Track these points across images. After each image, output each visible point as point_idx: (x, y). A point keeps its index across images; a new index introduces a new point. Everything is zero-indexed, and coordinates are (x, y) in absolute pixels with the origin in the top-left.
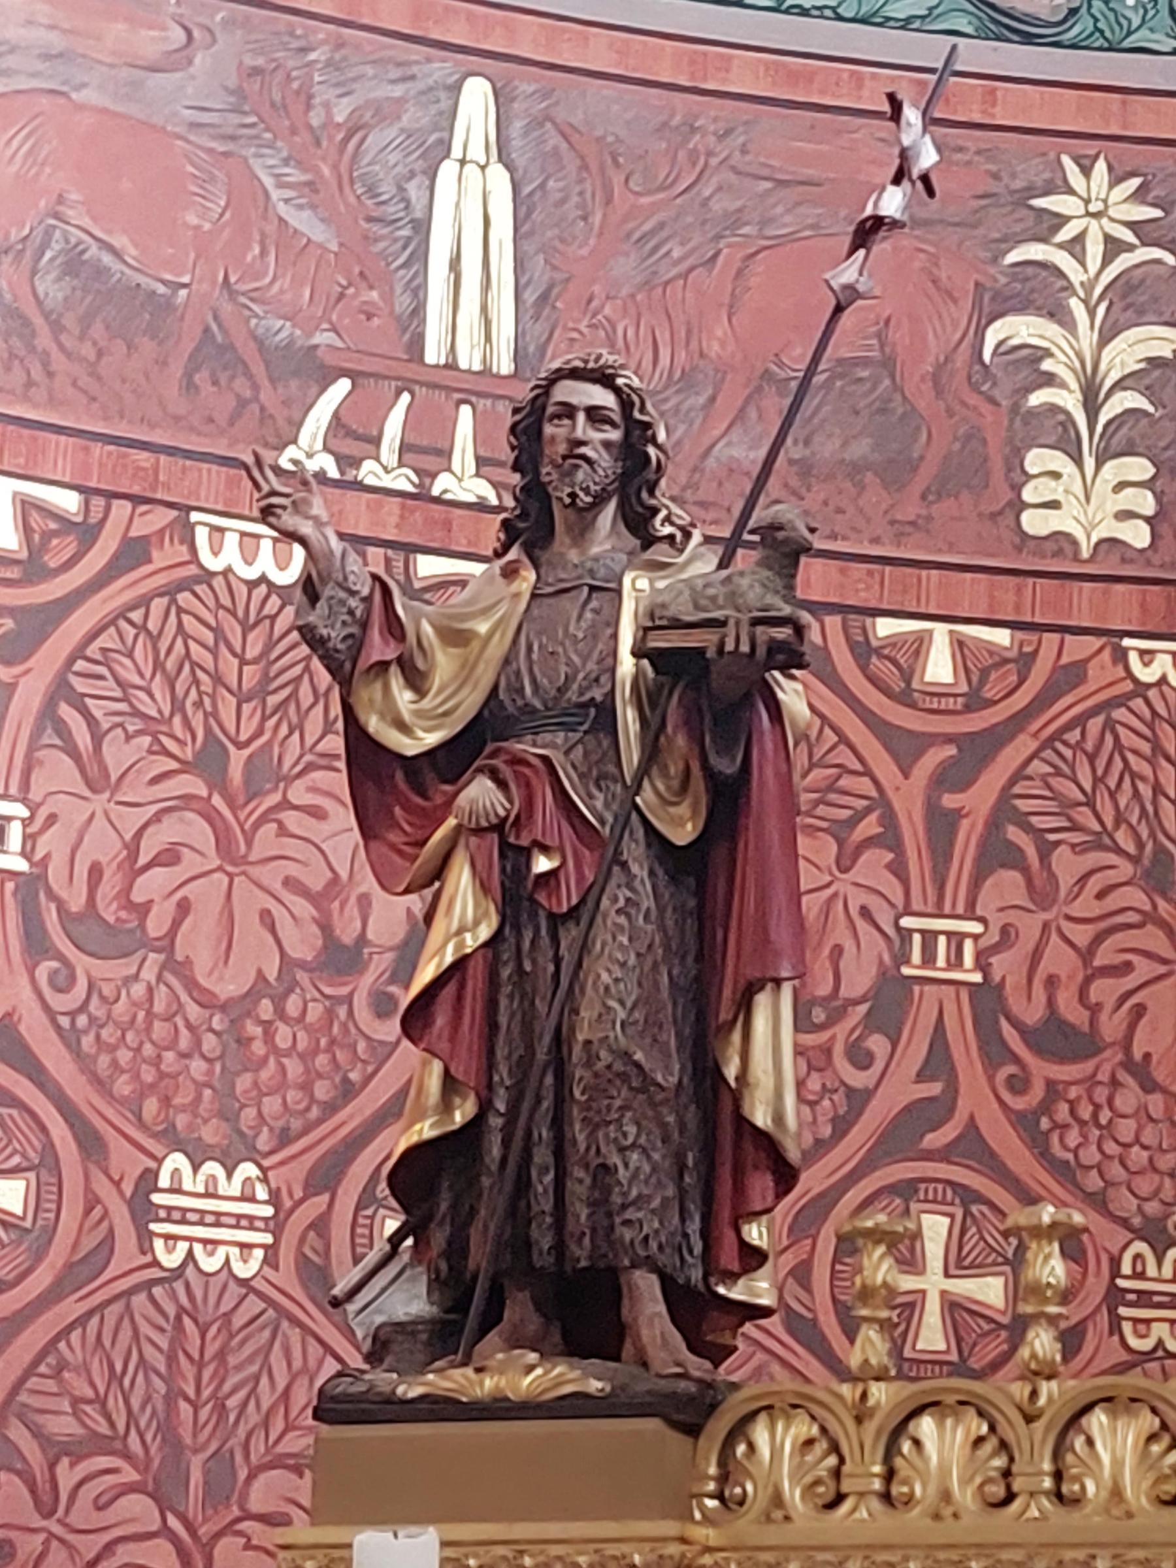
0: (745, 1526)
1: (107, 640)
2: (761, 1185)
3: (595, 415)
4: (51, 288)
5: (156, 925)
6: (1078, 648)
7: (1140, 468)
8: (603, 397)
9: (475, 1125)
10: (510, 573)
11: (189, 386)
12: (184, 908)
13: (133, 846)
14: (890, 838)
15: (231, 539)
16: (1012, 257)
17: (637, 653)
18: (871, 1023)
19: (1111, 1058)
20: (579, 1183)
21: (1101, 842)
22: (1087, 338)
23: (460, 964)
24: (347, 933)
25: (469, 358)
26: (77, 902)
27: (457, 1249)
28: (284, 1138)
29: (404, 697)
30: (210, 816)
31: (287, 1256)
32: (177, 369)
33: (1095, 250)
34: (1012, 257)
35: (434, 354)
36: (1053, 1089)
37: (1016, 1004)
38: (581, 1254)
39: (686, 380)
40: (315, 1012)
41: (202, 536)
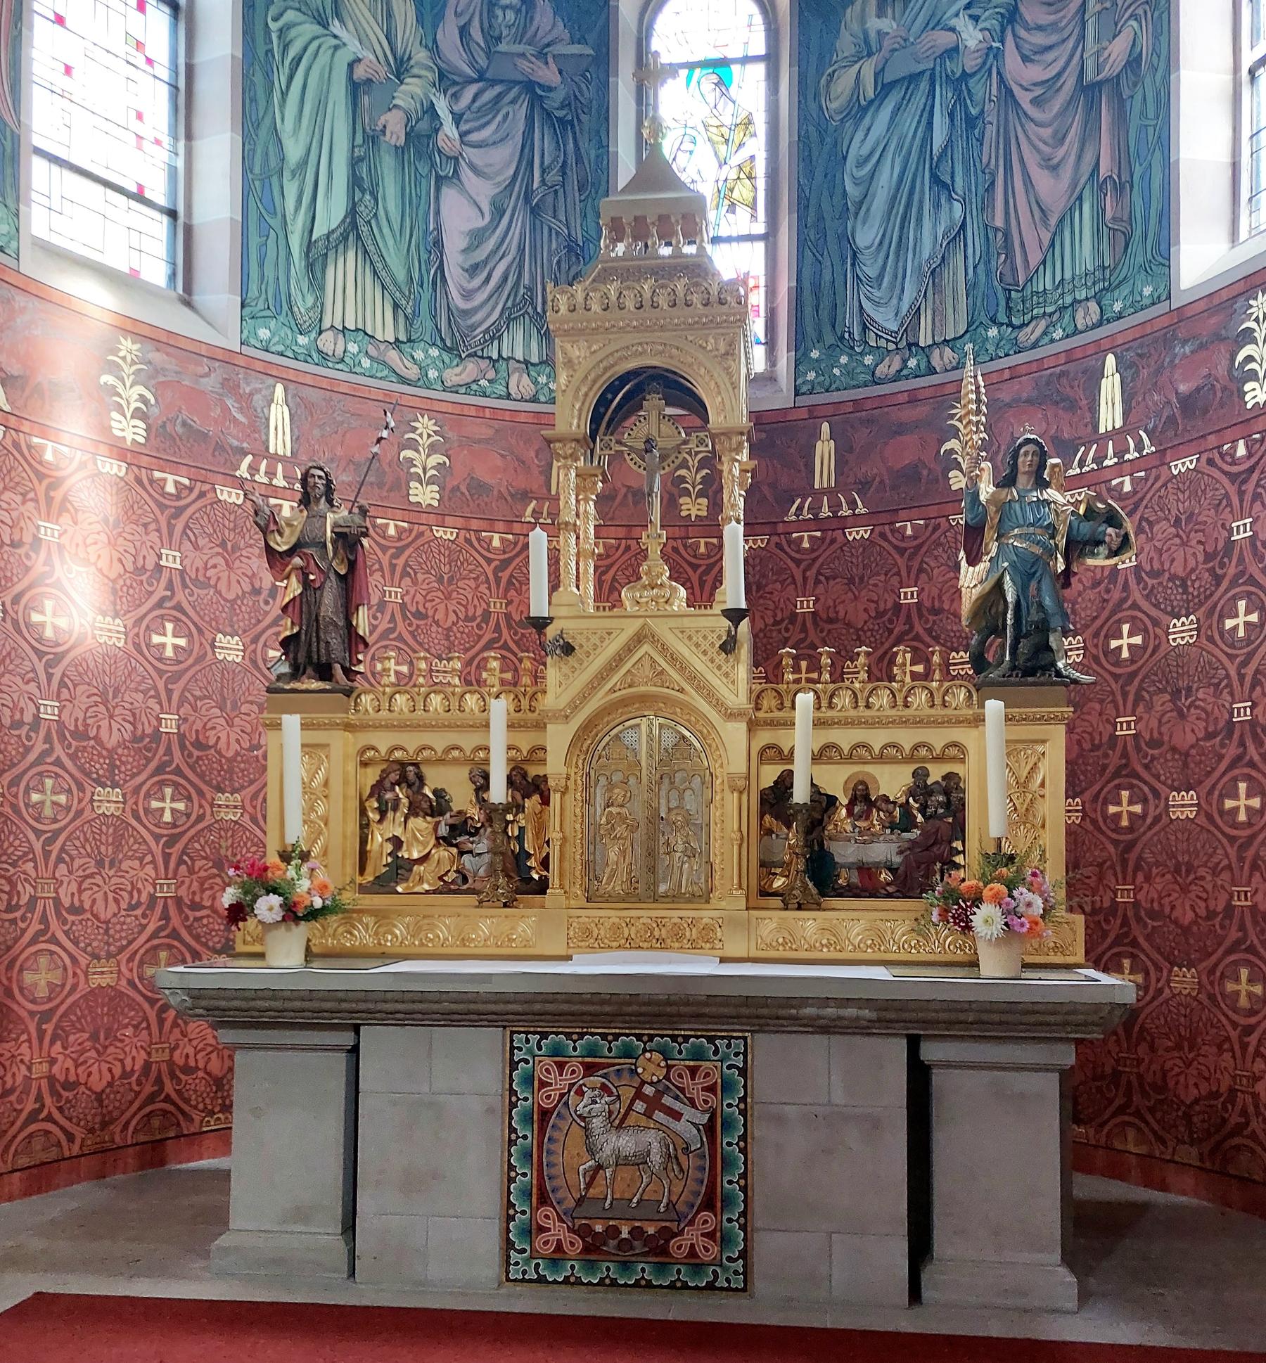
0: (360, 715)
1: (197, 515)
2: (361, 647)
3: (320, 477)
4: (179, 429)
5: (212, 582)
6: (423, 528)
7: (436, 488)
8: (322, 474)
9: (298, 633)
10: (301, 511)
11: (214, 456)
12: (219, 579)
13: (206, 564)
14: (381, 569)
15: (225, 493)
16: (406, 436)
17: (332, 532)
18: (377, 611)
19: (430, 620)
20: (322, 645)
21: (428, 572)
22: (424, 457)
23: (294, 598)
24: (257, 586)
25: (280, 452)
26: (193, 576)
27: (295, 659)
28: (245, 632)
29: (278, 538)
30: (224, 558)
31: (129, 641)
32: (211, 451)
33: (425, 436)
34: (406, 436)
35: (272, 450)
36: (418, 626)
37: (409, 606)
38: (324, 659)
39: (332, 460)
40: (251, 603)
41: (218, 492)
